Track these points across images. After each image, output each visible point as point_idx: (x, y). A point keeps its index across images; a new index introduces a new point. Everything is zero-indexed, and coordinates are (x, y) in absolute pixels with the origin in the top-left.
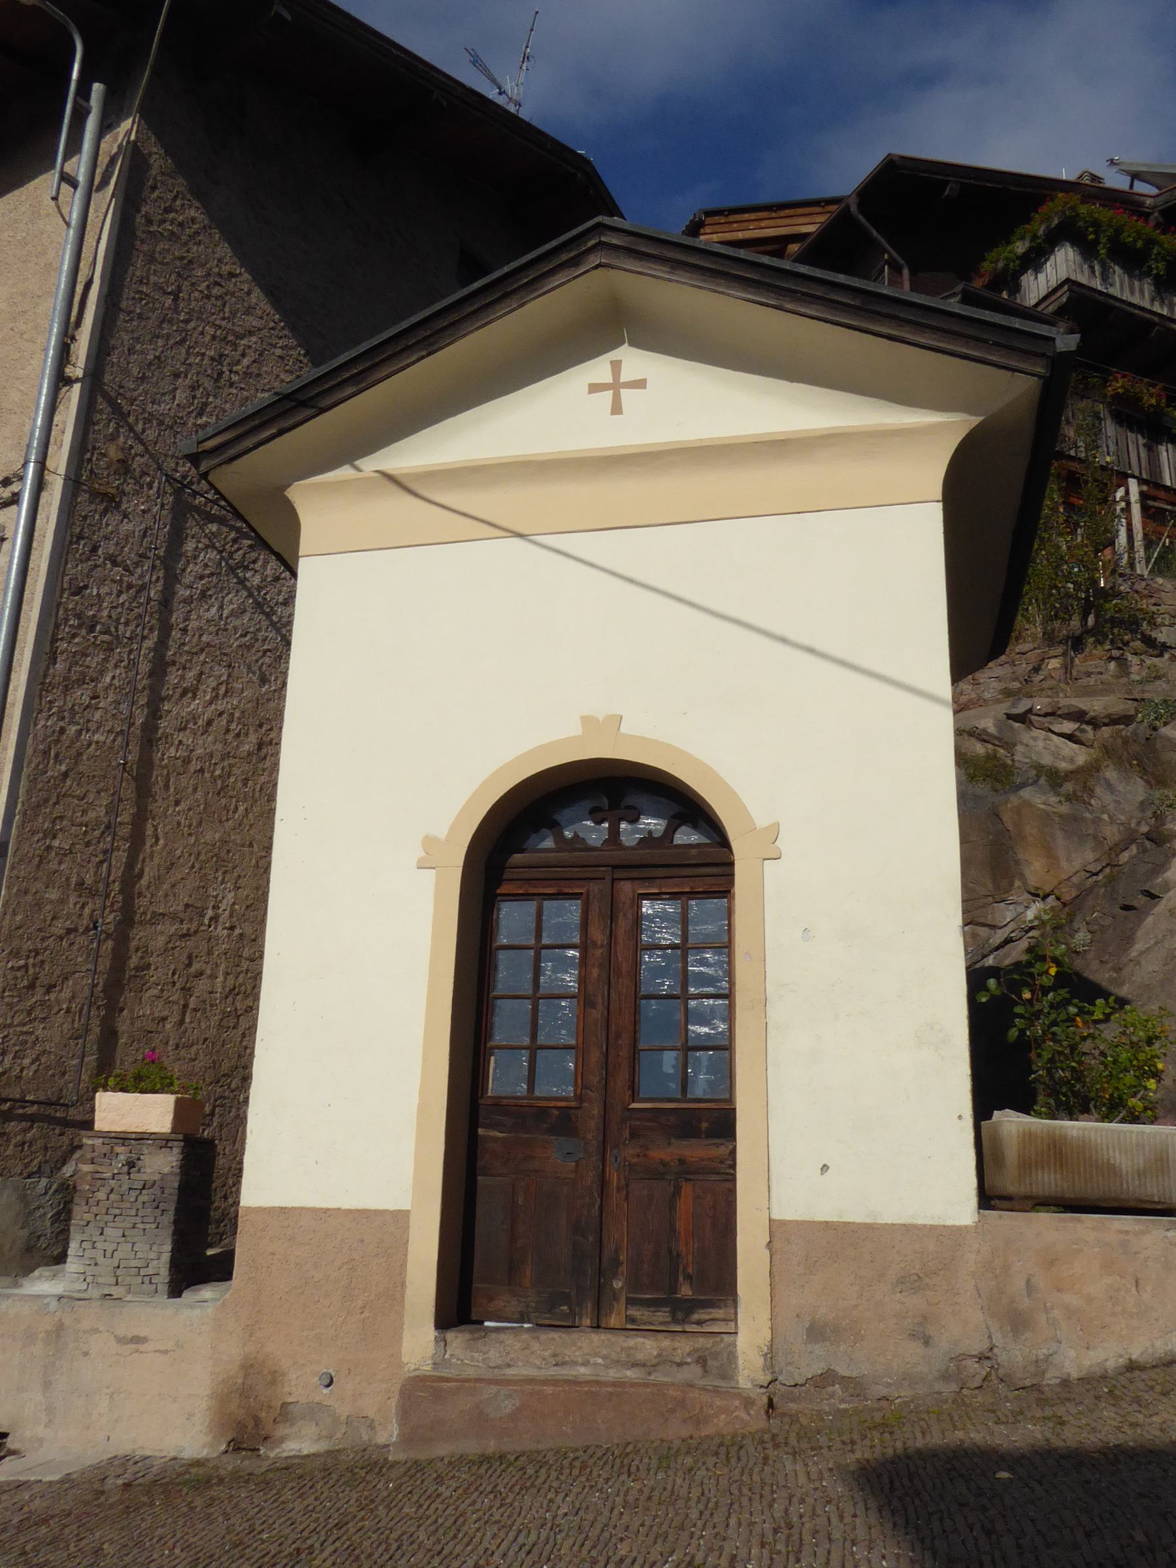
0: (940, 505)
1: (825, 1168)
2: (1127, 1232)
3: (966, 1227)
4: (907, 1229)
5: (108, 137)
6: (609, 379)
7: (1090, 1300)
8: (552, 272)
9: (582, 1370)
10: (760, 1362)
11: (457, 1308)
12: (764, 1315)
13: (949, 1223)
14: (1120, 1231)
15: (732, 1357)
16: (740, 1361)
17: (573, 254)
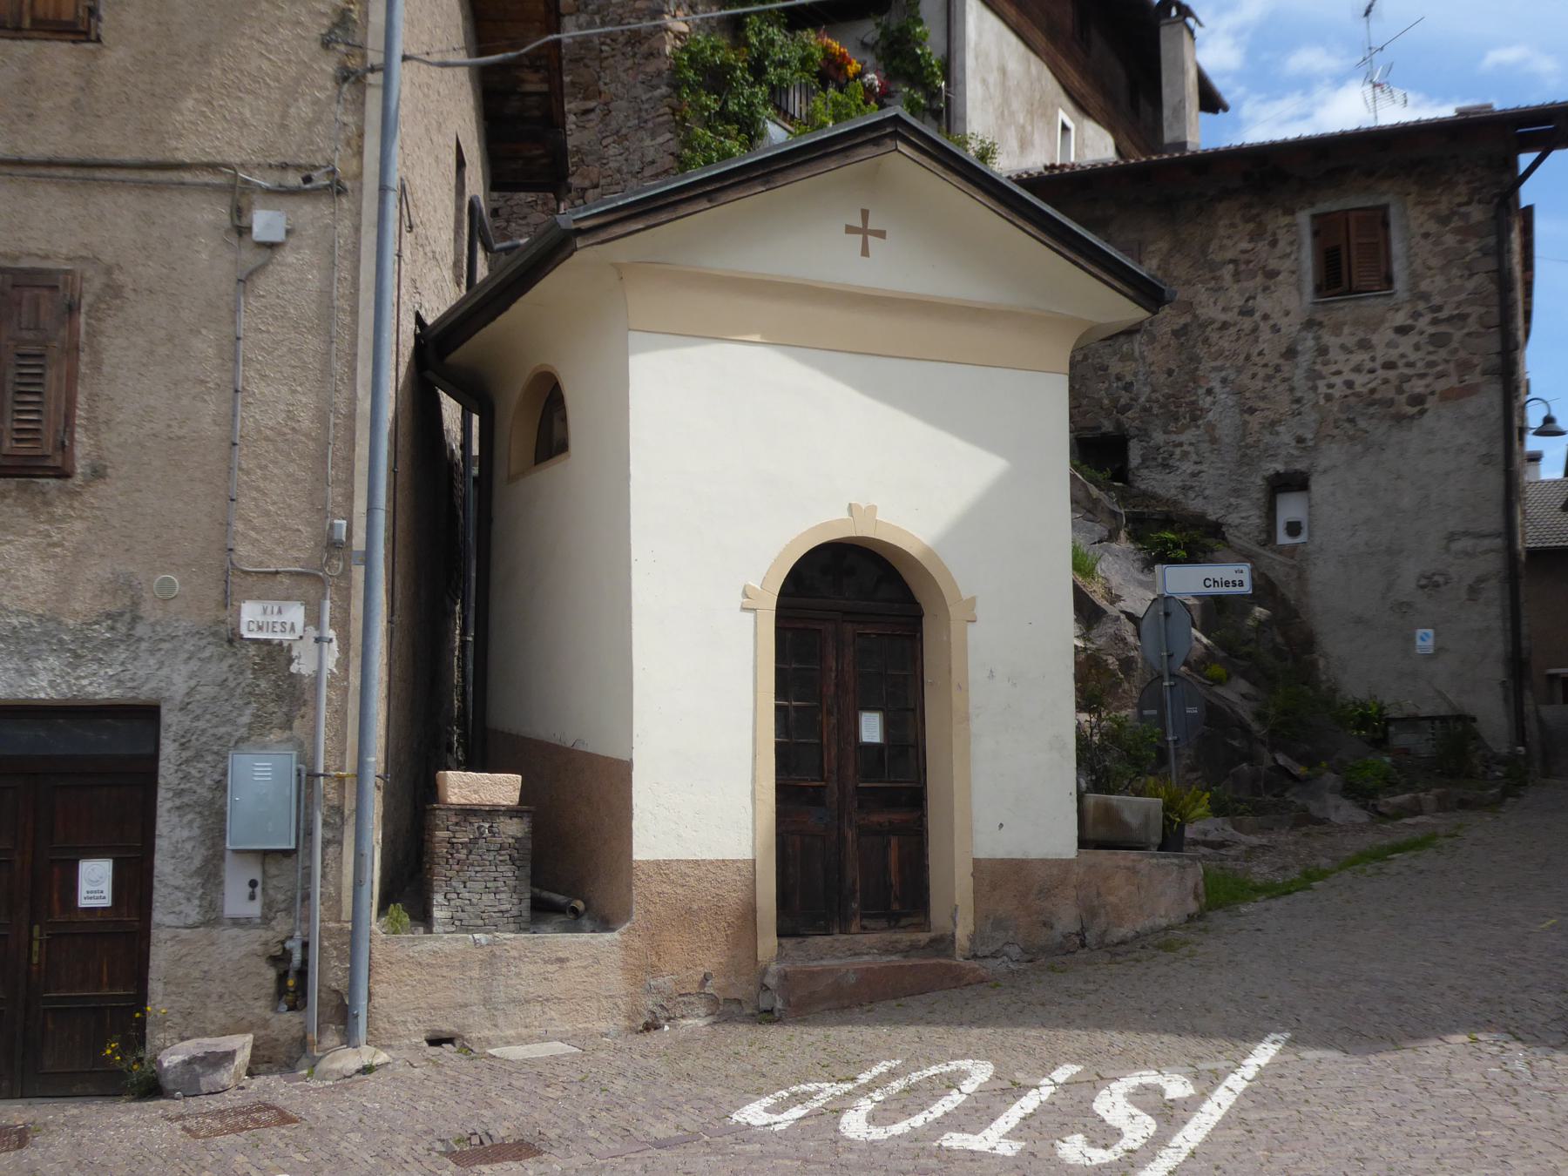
4: (1044, 861)
5: (1528, 694)
6: (860, 225)
9: (866, 958)
10: (967, 944)
12: (970, 918)
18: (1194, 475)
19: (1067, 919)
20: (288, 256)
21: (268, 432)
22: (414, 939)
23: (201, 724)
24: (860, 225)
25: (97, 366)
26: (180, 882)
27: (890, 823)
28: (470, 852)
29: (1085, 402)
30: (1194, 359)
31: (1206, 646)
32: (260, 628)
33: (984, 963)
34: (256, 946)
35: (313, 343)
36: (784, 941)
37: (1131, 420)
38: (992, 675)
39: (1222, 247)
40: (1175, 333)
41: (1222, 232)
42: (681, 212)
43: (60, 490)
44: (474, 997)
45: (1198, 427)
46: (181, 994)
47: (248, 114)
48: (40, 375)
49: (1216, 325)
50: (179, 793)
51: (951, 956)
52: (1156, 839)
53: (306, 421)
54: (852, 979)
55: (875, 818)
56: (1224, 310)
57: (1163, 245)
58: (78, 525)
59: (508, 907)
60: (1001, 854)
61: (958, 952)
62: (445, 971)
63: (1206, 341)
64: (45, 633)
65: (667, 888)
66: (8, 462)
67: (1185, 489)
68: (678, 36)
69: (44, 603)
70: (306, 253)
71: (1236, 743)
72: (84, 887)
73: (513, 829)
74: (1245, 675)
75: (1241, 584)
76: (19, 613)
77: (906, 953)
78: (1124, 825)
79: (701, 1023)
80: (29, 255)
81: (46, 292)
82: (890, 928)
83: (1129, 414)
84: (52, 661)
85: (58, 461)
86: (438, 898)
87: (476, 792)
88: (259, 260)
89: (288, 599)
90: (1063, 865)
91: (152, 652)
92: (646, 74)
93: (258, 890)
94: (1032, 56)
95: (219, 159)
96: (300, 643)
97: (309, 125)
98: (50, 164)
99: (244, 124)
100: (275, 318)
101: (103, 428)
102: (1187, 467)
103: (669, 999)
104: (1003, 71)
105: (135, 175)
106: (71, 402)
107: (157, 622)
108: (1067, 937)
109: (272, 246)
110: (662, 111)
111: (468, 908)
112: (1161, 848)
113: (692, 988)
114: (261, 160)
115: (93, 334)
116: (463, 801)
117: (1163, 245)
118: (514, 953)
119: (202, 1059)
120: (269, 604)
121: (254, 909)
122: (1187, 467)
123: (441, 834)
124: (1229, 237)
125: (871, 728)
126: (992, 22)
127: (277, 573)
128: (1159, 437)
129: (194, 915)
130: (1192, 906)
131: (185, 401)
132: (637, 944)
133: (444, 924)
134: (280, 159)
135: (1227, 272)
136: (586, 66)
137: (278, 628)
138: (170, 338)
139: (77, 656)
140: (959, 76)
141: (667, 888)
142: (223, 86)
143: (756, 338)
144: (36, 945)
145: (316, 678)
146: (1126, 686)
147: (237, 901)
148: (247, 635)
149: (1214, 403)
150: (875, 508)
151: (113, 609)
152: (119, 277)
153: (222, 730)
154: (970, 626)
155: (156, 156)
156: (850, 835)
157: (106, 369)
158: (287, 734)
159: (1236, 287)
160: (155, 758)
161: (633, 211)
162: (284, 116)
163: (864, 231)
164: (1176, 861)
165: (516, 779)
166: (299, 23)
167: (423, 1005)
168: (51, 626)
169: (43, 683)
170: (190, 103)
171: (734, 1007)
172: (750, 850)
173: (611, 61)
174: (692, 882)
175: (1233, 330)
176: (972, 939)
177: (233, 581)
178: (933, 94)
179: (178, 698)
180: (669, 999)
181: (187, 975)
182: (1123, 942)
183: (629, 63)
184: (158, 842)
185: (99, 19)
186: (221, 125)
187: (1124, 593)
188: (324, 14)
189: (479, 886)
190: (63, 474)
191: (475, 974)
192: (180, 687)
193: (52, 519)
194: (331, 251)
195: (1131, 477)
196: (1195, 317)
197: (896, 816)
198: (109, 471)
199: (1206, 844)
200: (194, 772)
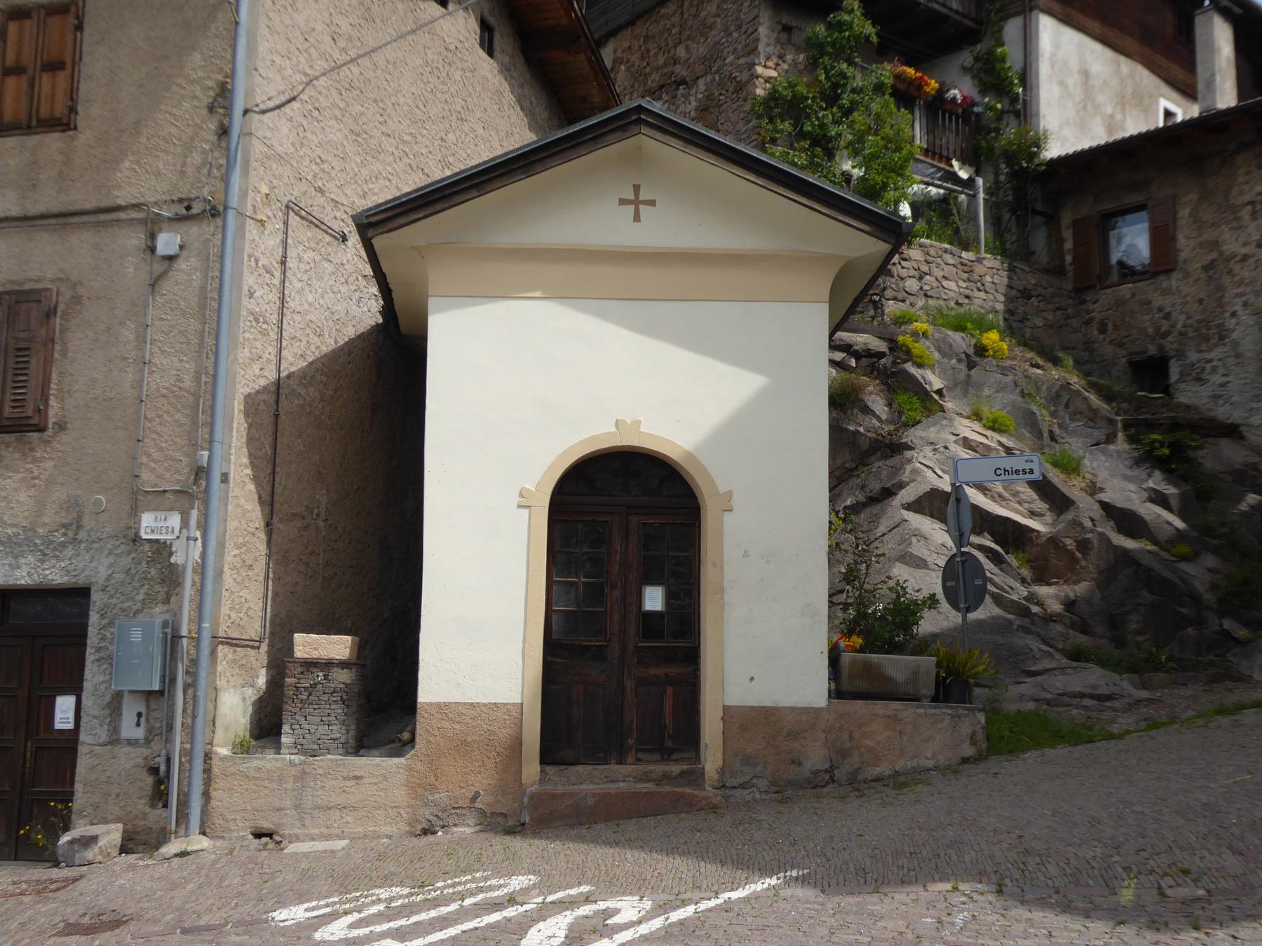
0: (827, 305)
1: (752, 679)
4: (793, 709)
6: (632, 197)
9: (622, 784)
10: (716, 777)
11: (548, 756)
15: (703, 774)
18: (1223, 385)
19: (815, 757)
20: (182, 265)
21: (165, 391)
23: (114, 601)
24: (632, 197)
25: (64, 354)
26: (96, 713)
27: (666, 675)
29: (1134, 332)
30: (1221, 288)
31: (1177, 529)
32: (153, 531)
33: (734, 792)
34: (140, 760)
35: (195, 324)
36: (548, 768)
37: (1170, 343)
38: (746, 554)
39: (1241, 193)
40: (1205, 268)
41: (1241, 179)
43: (39, 439)
44: (287, 803)
45: (1225, 345)
46: (93, 793)
47: (161, 167)
48: (27, 362)
49: (1238, 258)
50: (99, 650)
51: (701, 786)
52: (929, 691)
53: (188, 383)
54: (590, 801)
55: (653, 671)
56: (1245, 244)
57: (1193, 196)
58: (50, 464)
62: (266, 783)
63: (1230, 272)
64: (27, 539)
65: (446, 724)
66: (8, 423)
67: (1215, 397)
68: (768, 80)
69: (26, 518)
70: (193, 261)
71: (1184, 610)
72: (58, 715)
73: (343, 677)
74: (1216, 551)
75: (1031, 472)
76: (14, 525)
77: (659, 782)
78: (889, 680)
79: (468, 830)
80: (31, 280)
81: (35, 305)
82: (663, 760)
83: (1170, 338)
84: (31, 558)
85: (35, 421)
87: (316, 649)
88: (164, 268)
89: (171, 509)
90: (815, 712)
91: (88, 550)
93: (143, 720)
94: (1122, 59)
95: (142, 200)
96: (177, 542)
97: (199, 168)
98: (43, 217)
99: (158, 174)
100: (172, 309)
101: (66, 395)
102: (1217, 379)
103: (444, 811)
104: (1086, 74)
105: (92, 218)
106: (46, 380)
107: (92, 529)
108: (816, 773)
109: (171, 258)
111: (307, 736)
113: (466, 803)
114: (168, 198)
115: (64, 330)
117: (1193, 196)
118: (320, 771)
119: (79, 840)
120: (162, 515)
121: (139, 733)
122: (1217, 379)
124: (1247, 183)
125: (654, 599)
126: (1071, 37)
127: (165, 491)
128: (1193, 356)
129: (104, 737)
131: (114, 373)
132: (419, 766)
133: (289, 748)
134: (179, 195)
135: (1245, 213)
137: (164, 531)
138: (108, 329)
139: (45, 555)
140: (1034, 82)
141: (446, 724)
142: (147, 148)
143: (538, 294)
144: (29, 754)
145: (184, 567)
146: (1083, 563)
147: (130, 729)
148: (144, 537)
149: (1238, 324)
150: (639, 422)
151: (65, 521)
152: (81, 290)
153: (126, 604)
155: (105, 203)
156: (629, 685)
157: (69, 354)
158: (167, 607)
159: (1254, 224)
160: (85, 626)
162: (184, 164)
163: (636, 202)
165: (347, 639)
166: (195, 97)
168: (30, 533)
169: (24, 574)
170: (127, 164)
171: (500, 819)
174: (468, 719)
175: (1252, 261)
176: (721, 772)
177: (138, 500)
178: (1015, 99)
179: (101, 582)
180: (444, 811)
181: (97, 779)
182: (877, 780)
183: (735, 106)
184: (85, 684)
185: (77, 113)
186: (142, 180)
187: (1107, 486)
188: (211, 88)
190: (41, 429)
191: (289, 786)
192: (103, 573)
193: (35, 461)
194: (208, 259)
195: (1172, 391)
196: (1221, 253)
197: (673, 670)
198: (68, 425)
199: (1092, 697)
200: (108, 635)
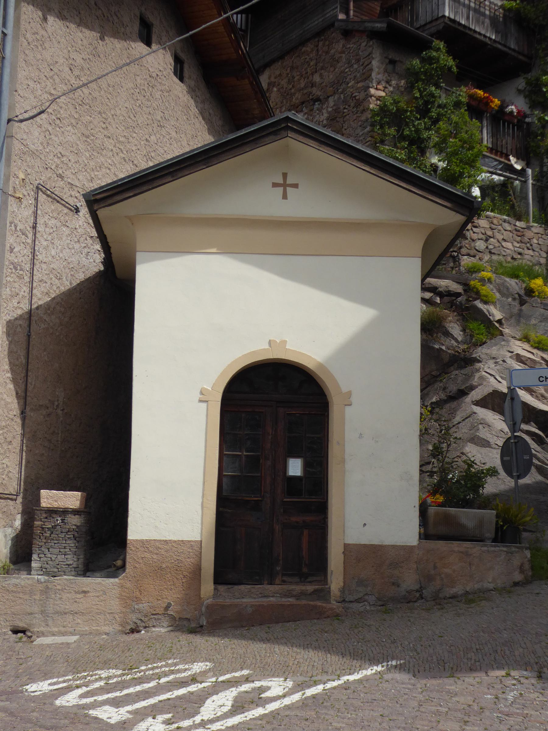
1: (365, 525)
2: (468, 548)
3: (415, 546)
4: (393, 547)
6: (281, 182)
7: (454, 571)
8: (263, 136)
9: (272, 599)
10: (338, 594)
11: (220, 578)
12: (341, 578)
13: (409, 544)
14: (465, 547)
16: (332, 594)
17: (274, 129)
19: (409, 581)
22: (5, 578)
24: (281, 182)
28: (52, 533)
42: (155, 184)
44: (36, 609)
51: (328, 601)
52: (490, 534)
54: (250, 610)
55: (294, 519)
59: (71, 562)
60: (364, 541)
61: (333, 598)
62: (21, 595)
65: (147, 555)
68: (379, 98)
73: (75, 521)
79: (163, 630)
86: (35, 557)
87: (56, 501)
90: (410, 549)
92: (361, 121)
108: (409, 592)
110: (368, 140)
111: (50, 562)
112: (495, 540)
113: (161, 611)
116: (49, 506)
118: (59, 587)
123: (37, 523)
125: (295, 467)
130: (518, 577)
132: (128, 585)
133: (37, 570)
136: (337, 122)
141: (147, 555)
143: (214, 250)
154: (347, 408)
161: (127, 187)
163: (285, 185)
164: (505, 549)
167: (9, 612)
172: (199, 535)
173: (347, 117)
174: (163, 552)
176: (343, 590)
180: (146, 616)
189: (56, 551)
